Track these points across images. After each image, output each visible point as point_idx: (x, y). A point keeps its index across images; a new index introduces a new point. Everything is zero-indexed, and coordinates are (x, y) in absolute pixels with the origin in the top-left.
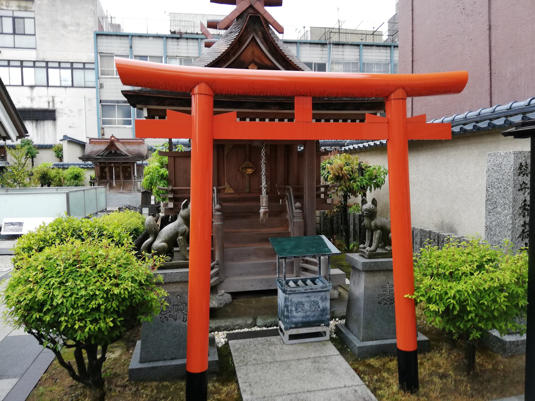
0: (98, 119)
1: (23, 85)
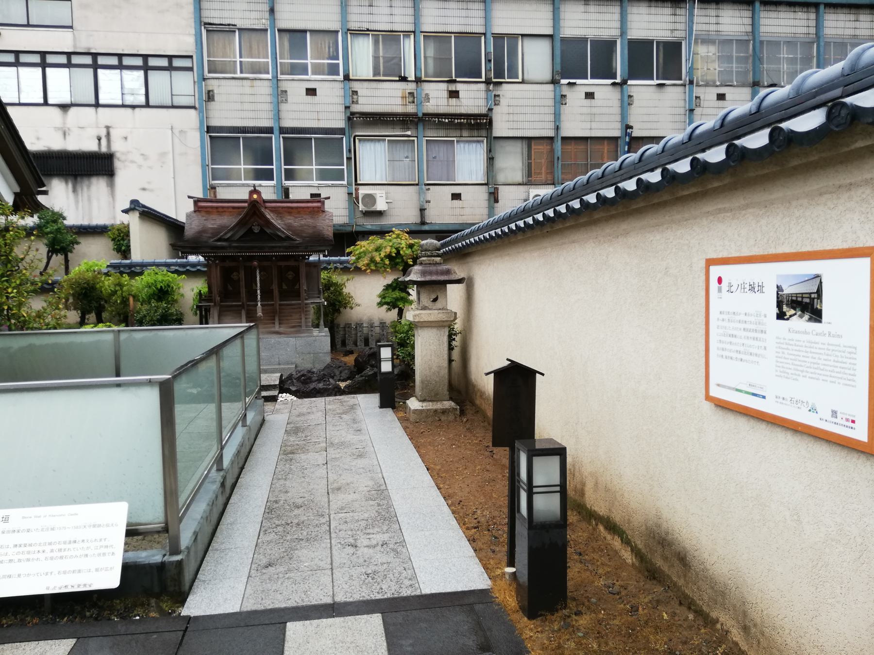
0: (204, 166)
1: (46, 103)
